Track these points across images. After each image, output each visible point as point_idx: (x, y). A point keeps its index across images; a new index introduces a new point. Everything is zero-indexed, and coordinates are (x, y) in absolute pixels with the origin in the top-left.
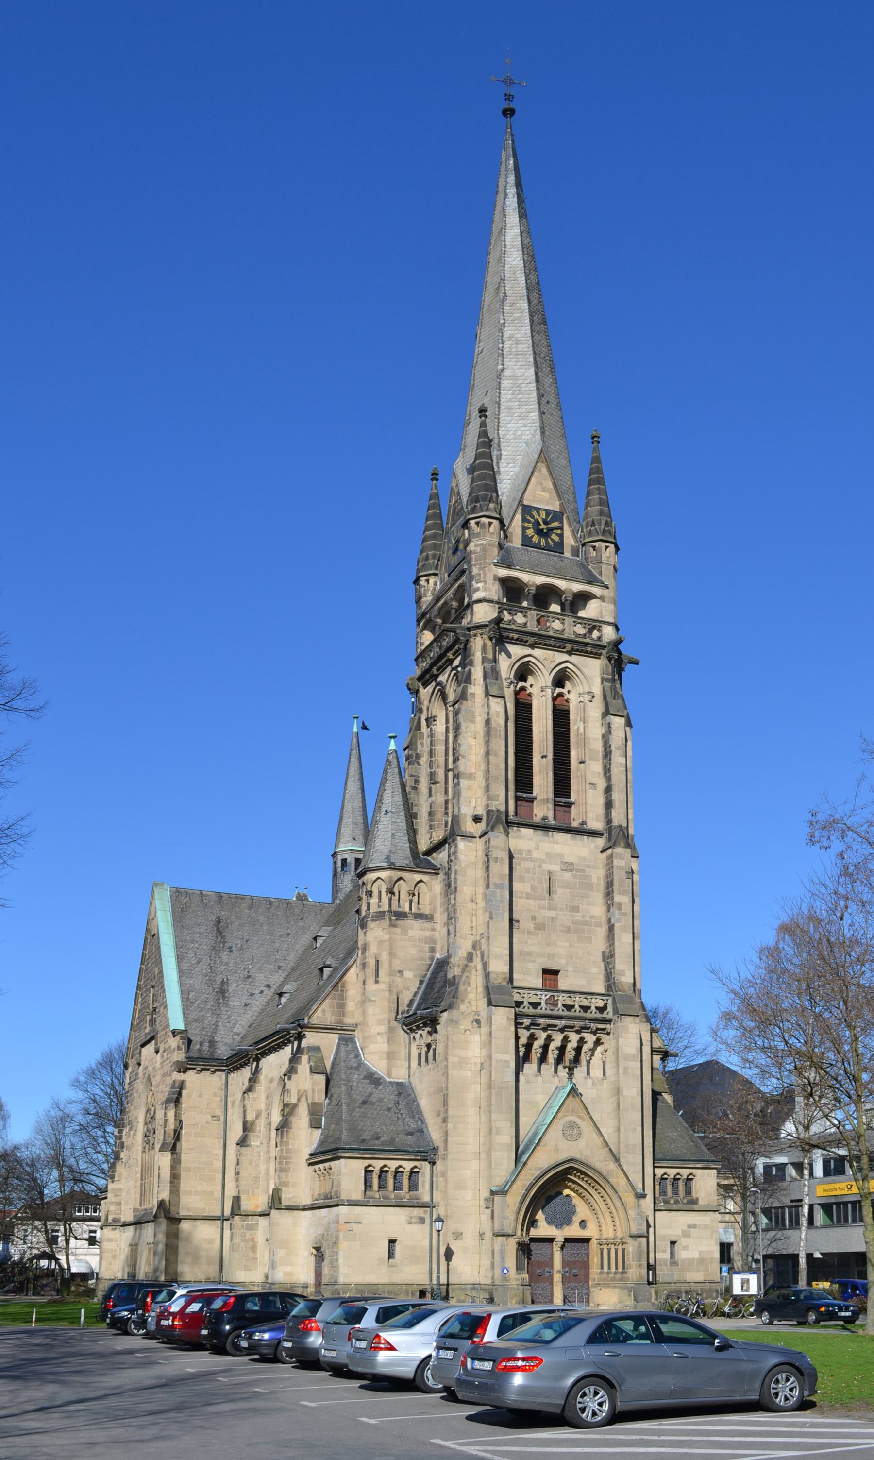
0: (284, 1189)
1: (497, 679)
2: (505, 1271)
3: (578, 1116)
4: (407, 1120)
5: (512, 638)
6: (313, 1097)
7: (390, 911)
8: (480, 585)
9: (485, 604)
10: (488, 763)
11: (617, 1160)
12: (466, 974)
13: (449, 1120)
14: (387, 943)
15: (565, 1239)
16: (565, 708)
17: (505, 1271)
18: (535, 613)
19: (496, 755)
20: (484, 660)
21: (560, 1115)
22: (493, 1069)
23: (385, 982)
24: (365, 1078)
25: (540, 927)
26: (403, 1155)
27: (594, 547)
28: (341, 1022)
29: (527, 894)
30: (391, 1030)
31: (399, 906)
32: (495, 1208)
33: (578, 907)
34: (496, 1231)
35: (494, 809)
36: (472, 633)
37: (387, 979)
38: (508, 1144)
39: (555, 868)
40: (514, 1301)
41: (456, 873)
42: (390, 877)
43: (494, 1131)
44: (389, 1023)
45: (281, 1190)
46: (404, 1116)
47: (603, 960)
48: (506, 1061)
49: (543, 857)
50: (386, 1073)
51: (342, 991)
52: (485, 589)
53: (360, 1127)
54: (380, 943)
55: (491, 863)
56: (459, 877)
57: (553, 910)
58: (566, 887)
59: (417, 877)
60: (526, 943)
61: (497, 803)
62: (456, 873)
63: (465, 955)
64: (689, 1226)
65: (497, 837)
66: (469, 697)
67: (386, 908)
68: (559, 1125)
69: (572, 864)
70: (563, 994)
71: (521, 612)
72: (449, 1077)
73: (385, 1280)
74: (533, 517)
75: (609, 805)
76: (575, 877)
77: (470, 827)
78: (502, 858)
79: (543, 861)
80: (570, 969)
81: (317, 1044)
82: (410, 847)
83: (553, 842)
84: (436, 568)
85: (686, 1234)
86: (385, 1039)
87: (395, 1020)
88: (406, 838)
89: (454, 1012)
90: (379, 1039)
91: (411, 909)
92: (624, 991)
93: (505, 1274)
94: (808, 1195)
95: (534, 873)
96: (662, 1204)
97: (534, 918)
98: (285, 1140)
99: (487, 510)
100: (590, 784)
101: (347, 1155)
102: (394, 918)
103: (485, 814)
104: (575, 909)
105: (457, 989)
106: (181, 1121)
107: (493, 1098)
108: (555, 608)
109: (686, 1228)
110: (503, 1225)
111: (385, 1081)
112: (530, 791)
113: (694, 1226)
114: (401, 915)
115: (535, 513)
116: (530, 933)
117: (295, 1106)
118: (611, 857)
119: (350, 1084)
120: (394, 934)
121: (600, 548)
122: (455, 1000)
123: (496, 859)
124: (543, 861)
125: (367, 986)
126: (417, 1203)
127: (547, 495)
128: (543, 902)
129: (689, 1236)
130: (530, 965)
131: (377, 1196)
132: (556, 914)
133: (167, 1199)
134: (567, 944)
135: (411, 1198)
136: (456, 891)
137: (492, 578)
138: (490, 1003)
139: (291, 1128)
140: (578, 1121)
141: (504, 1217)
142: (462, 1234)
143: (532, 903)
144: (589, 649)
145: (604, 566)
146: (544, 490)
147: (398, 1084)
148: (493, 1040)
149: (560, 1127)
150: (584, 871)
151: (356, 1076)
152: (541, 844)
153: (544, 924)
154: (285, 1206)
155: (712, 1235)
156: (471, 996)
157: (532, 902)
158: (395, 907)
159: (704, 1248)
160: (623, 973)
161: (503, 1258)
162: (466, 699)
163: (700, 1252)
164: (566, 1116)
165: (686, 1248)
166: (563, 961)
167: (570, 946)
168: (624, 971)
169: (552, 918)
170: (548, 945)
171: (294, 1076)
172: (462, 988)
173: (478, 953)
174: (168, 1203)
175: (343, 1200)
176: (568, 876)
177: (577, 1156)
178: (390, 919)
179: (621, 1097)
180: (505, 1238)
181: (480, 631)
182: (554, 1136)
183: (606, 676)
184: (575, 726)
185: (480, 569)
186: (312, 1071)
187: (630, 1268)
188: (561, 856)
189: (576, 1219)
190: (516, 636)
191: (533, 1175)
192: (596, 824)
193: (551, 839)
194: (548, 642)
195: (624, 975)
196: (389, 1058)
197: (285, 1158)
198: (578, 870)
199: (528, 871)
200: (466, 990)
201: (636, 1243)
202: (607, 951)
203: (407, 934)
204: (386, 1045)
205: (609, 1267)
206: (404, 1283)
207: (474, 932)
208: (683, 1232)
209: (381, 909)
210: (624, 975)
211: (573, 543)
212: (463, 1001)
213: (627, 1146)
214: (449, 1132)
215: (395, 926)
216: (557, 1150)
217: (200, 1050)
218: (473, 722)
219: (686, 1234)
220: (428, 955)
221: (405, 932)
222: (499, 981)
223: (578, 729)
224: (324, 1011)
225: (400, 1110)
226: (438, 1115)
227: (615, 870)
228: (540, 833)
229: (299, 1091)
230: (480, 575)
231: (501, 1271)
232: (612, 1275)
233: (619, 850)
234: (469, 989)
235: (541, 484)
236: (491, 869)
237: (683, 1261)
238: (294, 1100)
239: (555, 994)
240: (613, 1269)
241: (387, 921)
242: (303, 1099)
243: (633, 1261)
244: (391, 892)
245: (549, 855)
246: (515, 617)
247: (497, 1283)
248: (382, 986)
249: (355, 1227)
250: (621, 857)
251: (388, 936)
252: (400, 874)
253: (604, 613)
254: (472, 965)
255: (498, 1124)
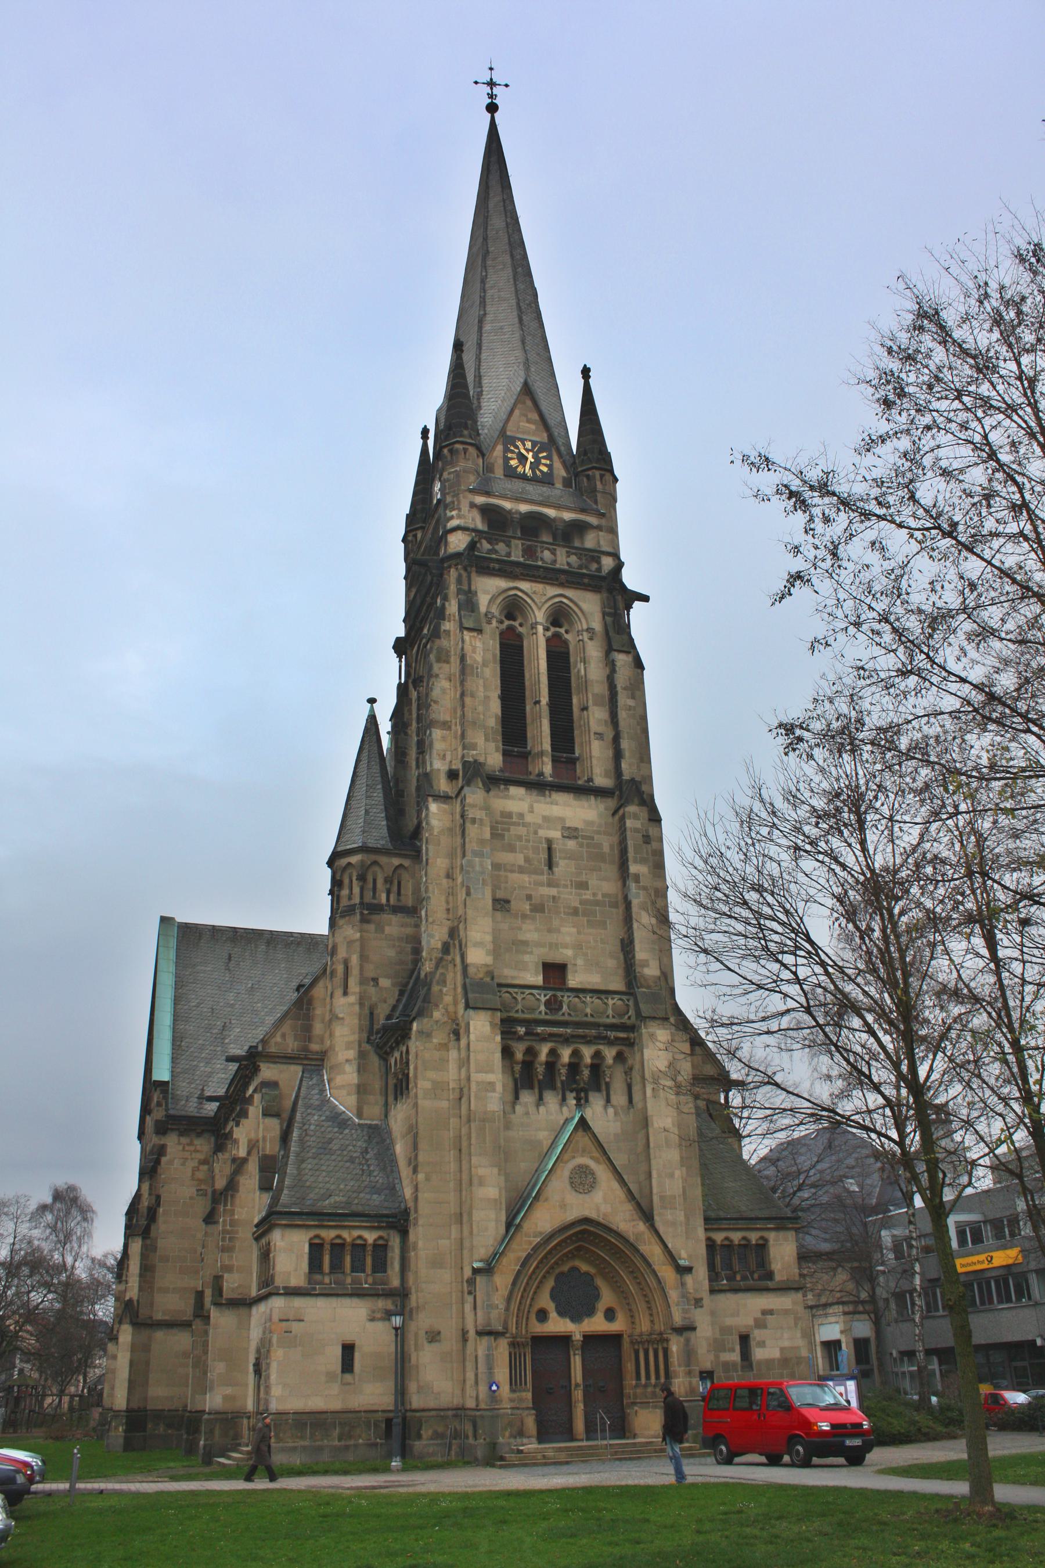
0: (226, 1276)
1: (473, 611)
2: (494, 1388)
3: (592, 1158)
4: (375, 1174)
5: (494, 569)
6: (264, 1149)
7: (362, 903)
8: (454, 513)
9: (460, 532)
10: (463, 706)
11: (647, 1216)
12: (440, 971)
13: (419, 1169)
14: (358, 944)
15: (584, 1336)
16: (562, 650)
17: (494, 1388)
18: (519, 542)
19: (472, 696)
20: (459, 591)
21: (566, 1157)
22: (472, 1094)
23: (354, 993)
24: (328, 1119)
25: (538, 908)
26: (363, 1221)
27: (588, 477)
28: (306, 1049)
29: (520, 867)
30: (362, 1055)
31: (374, 897)
32: (478, 1294)
33: (587, 883)
34: (480, 1328)
35: (471, 759)
36: (446, 565)
37: (357, 990)
38: (496, 1200)
39: (555, 834)
40: (507, 1434)
41: (427, 842)
42: (362, 861)
43: (475, 1181)
44: (360, 1046)
45: (222, 1277)
46: (372, 1168)
47: (623, 950)
48: (490, 1083)
49: (540, 821)
50: (355, 1112)
51: (308, 1009)
52: (459, 517)
53: (308, 1184)
54: (350, 943)
55: (468, 825)
56: (431, 847)
57: (554, 887)
58: (569, 858)
59: (396, 861)
60: (520, 929)
61: (474, 752)
62: (427, 842)
63: (439, 945)
64: (765, 1312)
65: (473, 793)
66: (443, 635)
67: (357, 900)
68: (565, 1171)
69: (576, 829)
70: (569, 994)
71: (504, 541)
72: (419, 1110)
73: (336, 1405)
74: (517, 447)
75: (618, 755)
76: (581, 845)
77: (443, 785)
78: (481, 820)
79: (540, 827)
80: (580, 962)
81: (274, 1078)
82: (388, 826)
83: (552, 803)
84: (424, 522)
85: (760, 1324)
86: (355, 1067)
87: (368, 1042)
88: (383, 815)
89: (425, 1020)
90: (348, 1068)
91: (388, 900)
92: (648, 987)
93: (494, 1391)
94: (917, 1260)
95: (528, 841)
96: (725, 1282)
97: (529, 897)
98: (229, 1207)
99: (462, 436)
100: (595, 733)
101: (284, 1222)
102: (366, 912)
103: (460, 767)
104: (583, 885)
105: (429, 989)
106: (158, 1197)
107: (473, 1135)
108: (546, 538)
109: (759, 1315)
110: (489, 1318)
111: (353, 1122)
112: (525, 745)
113: (771, 1312)
114: (376, 909)
115: (519, 443)
116: (524, 916)
117: (244, 1161)
118: (622, 819)
119: (306, 1127)
120: (367, 931)
121: (594, 476)
122: (426, 1005)
123: (474, 821)
124: (540, 827)
125: (334, 1000)
126: (383, 1289)
127: (533, 427)
128: (541, 877)
129: (765, 1326)
130: (527, 958)
131: (327, 1280)
132: (558, 892)
133: (135, 1298)
134: (574, 930)
135: (374, 1283)
136: (427, 864)
137: (468, 505)
138: (467, 1006)
139: (237, 1191)
140: (592, 1164)
141: (491, 1306)
142: (439, 1333)
143: (527, 879)
144: (586, 581)
145: (599, 495)
146: (529, 421)
147: (370, 1126)
148: (472, 1054)
149: (566, 1173)
150: (592, 838)
151: (316, 1117)
152: (535, 805)
153: (543, 906)
154: (227, 1299)
155: (796, 1324)
156: (448, 999)
157: (526, 878)
158: (368, 898)
159: (786, 1344)
160: (645, 964)
161: (490, 1368)
162: (439, 637)
163: (782, 1349)
164: (574, 1157)
165: (762, 1344)
166: (569, 953)
167: (579, 933)
168: (647, 961)
169: (554, 897)
170: (550, 931)
171: (243, 1121)
172: (435, 988)
173: (457, 942)
174: (135, 1303)
175: (278, 1288)
176: (571, 844)
177: (593, 1215)
178: (362, 914)
179: (651, 1130)
180: (492, 1338)
181: (454, 562)
182: (559, 1187)
183: (607, 610)
184: (578, 668)
185: (453, 496)
186: (266, 1114)
187: (677, 1377)
188: (562, 820)
189: (602, 1306)
190: (497, 566)
191: (530, 1243)
192: (601, 780)
193: (548, 799)
194: (536, 573)
195: (648, 966)
196: (359, 1092)
197: (228, 1232)
198: (584, 837)
199: (519, 838)
200: (441, 991)
201: (682, 1339)
202: (626, 936)
203: (383, 931)
204: (355, 1075)
205: (648, 1377)
206: (363, 1409)
207: (451, 916)
208: (756, 1320)
209: (352, 902)
210: (648, 966)
211: (563, 473)
212: (437, 1006)
213: (662, 1198)
214: (420, 1186)
215: (368, 922)
216: (563, 1206)
217: (185, 1106)
218: (448, 662)
219: (760, 1324)
220: (410, 957)
221: (380, 929)
222: (481, 975)
223: (579, 671)
224: (283, 1036)
225: (367, 1160)
226: (409, 1164)
227: (628, 833)
228: (535, 793)
229: (250, 1141)
230: (453, 502)
231: (487, 1388)
232: (650, 1389)
233: (632, 809)
234: (445, 990)
235: (526, 416)
236: (467, 832)
237: (759, 1362)
238: (242, 1153)
239: (559, 994)
240: (653, 1380)
241: (358, 917)
242: (255, 1151)
243: (680, 1365)
244: (362, 878)
245: (545, 819)
246: (496, 547)
247: (483, 1406)
248: (352, 999)
249: (295, 1327)
250: (636, 817)
251: (358, 935)
252: (374, 857)
253: (602, 543)
254: (449, 958)
255: (481, 1171)
